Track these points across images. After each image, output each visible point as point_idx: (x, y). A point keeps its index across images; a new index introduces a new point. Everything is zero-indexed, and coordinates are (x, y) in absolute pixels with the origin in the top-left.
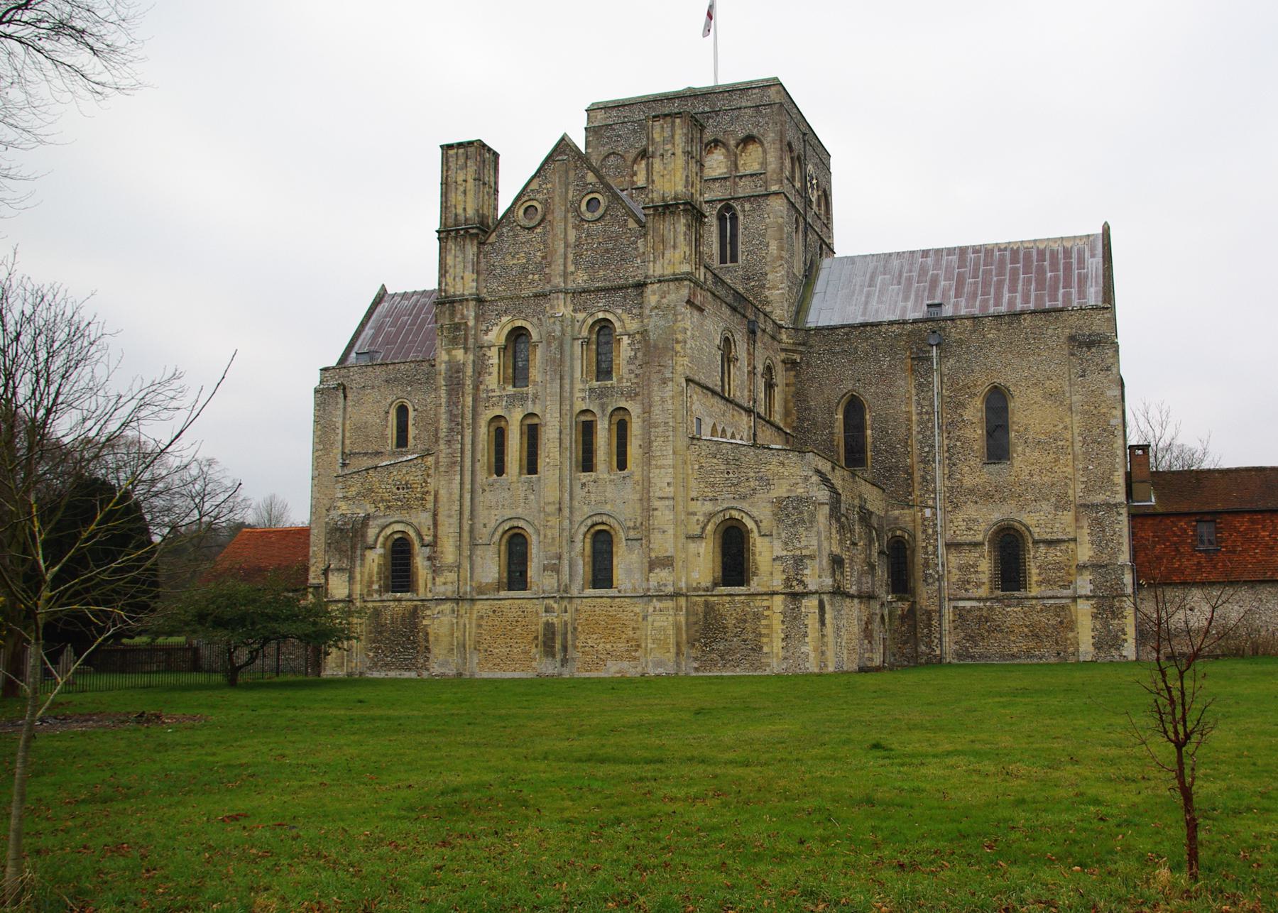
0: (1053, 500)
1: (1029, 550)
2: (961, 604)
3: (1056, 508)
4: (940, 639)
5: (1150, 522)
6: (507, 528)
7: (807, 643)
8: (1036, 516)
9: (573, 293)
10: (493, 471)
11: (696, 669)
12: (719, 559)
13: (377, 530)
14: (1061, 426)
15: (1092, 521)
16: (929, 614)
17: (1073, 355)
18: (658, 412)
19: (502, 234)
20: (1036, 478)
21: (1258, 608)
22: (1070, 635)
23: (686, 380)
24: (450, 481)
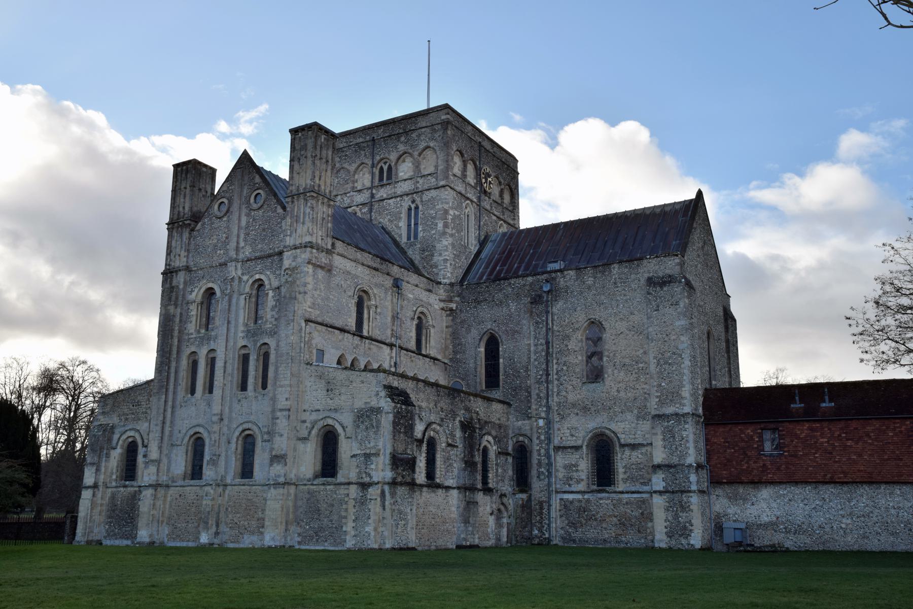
0: (636, 412)
1: (617, 453)
2: (566, 496)
3: (638, 418)
4: (549, 525)
5: (721, 430)
6: (192, 434)
7: (370, 524)
8: (622, 425)
9: (242, 261)
10: (189, 392)
11: (299, 543)
12: (319, 456)
13: (119, 435)
14: (641, 351)
15: (664, 428)
16: (541, 503)
17: (649, 293)
18: (283, 345)
19: (204, 223)
20: (622, 394)
21: (822, 506)
22: (650, 525)
23: (305, 321)
24: (159, 399)
